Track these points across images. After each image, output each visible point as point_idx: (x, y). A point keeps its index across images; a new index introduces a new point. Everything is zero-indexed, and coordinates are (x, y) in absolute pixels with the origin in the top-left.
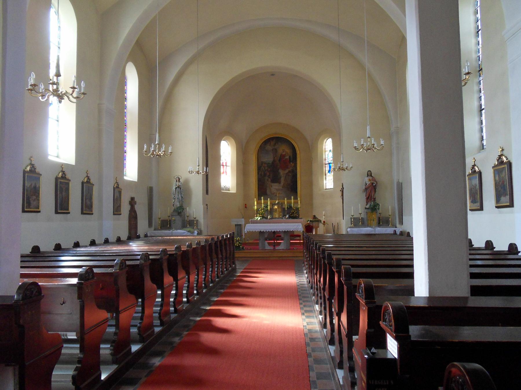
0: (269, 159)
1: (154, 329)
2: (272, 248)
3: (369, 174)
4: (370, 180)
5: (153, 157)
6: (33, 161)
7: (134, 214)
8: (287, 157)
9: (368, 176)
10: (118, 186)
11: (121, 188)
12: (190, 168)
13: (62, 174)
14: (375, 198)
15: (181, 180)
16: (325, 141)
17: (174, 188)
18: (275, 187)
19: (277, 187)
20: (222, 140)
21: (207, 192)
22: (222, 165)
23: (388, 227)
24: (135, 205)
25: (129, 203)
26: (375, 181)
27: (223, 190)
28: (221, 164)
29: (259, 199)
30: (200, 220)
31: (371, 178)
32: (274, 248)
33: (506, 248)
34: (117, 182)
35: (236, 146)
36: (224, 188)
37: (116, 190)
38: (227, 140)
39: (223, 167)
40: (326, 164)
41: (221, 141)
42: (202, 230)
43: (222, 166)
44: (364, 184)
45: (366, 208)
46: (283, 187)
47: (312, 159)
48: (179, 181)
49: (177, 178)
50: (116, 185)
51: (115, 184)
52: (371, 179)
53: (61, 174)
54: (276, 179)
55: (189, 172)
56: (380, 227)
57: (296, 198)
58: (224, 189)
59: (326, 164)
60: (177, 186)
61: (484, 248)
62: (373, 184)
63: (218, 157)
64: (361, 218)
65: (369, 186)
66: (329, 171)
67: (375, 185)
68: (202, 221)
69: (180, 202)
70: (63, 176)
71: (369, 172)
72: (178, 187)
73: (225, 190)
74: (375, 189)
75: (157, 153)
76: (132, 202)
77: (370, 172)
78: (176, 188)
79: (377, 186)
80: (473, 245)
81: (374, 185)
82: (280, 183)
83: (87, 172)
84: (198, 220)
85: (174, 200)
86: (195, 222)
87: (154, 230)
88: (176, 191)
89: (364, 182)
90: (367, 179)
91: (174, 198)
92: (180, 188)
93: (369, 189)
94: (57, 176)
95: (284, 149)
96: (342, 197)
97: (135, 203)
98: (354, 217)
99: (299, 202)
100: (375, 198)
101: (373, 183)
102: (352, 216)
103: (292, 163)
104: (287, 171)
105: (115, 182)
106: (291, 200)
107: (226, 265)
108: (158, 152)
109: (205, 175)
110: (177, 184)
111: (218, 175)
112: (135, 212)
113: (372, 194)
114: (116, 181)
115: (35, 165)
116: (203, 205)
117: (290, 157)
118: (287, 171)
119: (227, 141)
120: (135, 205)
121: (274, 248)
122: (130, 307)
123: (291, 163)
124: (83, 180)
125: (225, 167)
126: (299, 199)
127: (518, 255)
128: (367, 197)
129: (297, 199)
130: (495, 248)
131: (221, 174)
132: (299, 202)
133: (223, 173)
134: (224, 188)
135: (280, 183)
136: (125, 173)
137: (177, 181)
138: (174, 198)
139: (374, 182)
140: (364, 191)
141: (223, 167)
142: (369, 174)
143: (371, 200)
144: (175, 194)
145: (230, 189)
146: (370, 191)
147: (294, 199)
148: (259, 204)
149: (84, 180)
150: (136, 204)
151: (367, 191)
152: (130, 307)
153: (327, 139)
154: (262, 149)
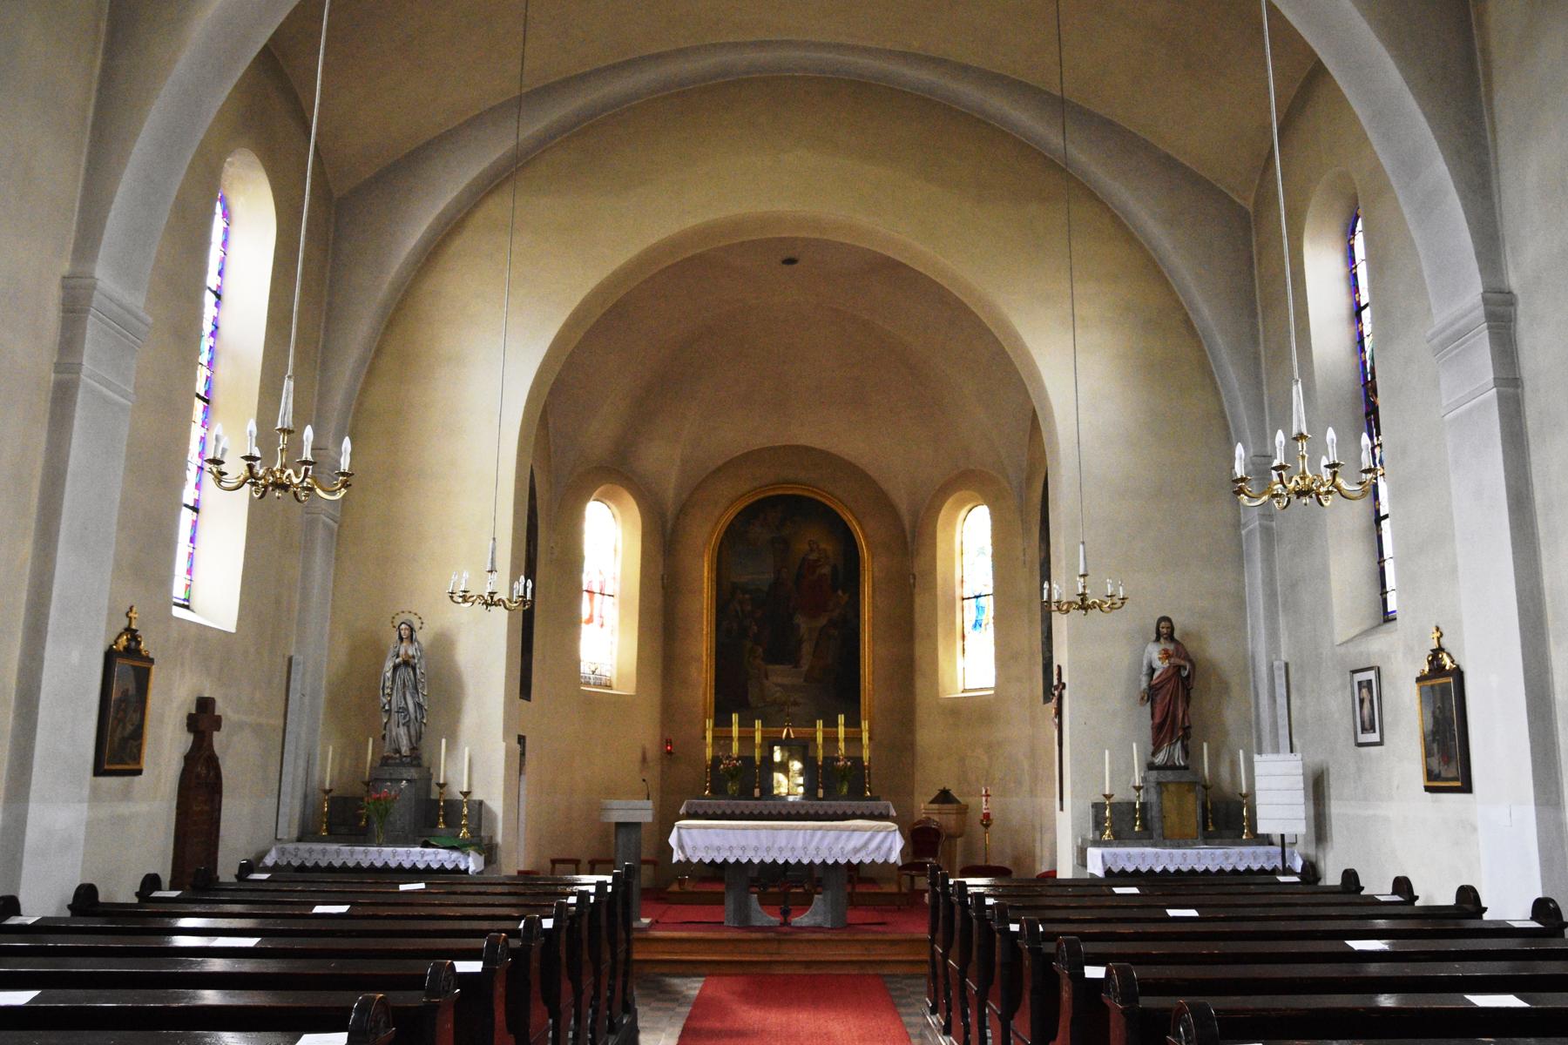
0: (757, 574)
1: (505, 876)
2: (775, 920)
3: (1165, 631)
4: (1166, 655)
5: (261, 497)
6: (134, 622)
7: (209, 772)
8: (826, 570)
9: (1158, 640)
10: (133, 644)
11: (151, 656)
12: (462, 579)
13: (127, 638)
14: (1187, 724)
15: (419, 635)
16: (963, 513)
17: (389, 665)
18: (779, 679)
19: (786, 681)
20: (593, 498)
21: (525, 691)
22: (587, 591)
23: (1238, 840)
24: (215, 733)
25: (185, 721)
26: (1187, 657)
27: (588, 684)
28: (585, 588)
29: (722, 721)
30: (489, 803)
31: (1171, 647)
32: (785, 920)
33: (1448, 899)
34: (134, 627)
35: (643, 523)
36: (592, 676)
37: (121, 665)
38: (610, 500)
39: (591, 600)
40: (963, 599)
41: (588, 500)
42: (497, 845)
43: (585, 595)
44: (1145, 669)
45: (1151, 767)
46: (805, 680)
47: (915, 578)
48: (411, 639)
49: (403, 626)
50: (123, 641)
51: (120, 636)
52: (1171, 653)
53: (125, 637)
54: (782, 651)
55: (451, 597)
56: (1209, 841)
57: (853, 722)
58: (592, 681)
59: (963, 599)
60: (398, 661)
61: (1340, 889)
62: (1179, 670)
63: (571, 562)
64: (1140, 803)
65: (1164, 677)
66: (977, 624)
67: (1188, 676)
68: (496, 802)
69: (408, 727)
70: (129, 644)
71: (1163, 624)
72: (406, 663)
73: (595, 685)
74: (1188, 690)
75: (278, 474)
76: (203, 719)
77: (1168, 624)
78: (396, 668)
79: (1194, 678)
80: (1363, 888)
81: (1185, 673)
82: (797, 664)
83: (130, 615)
84: (481, 803)
85: (387, 716)
86: (465, 811)
87: (299, 840)
88: (393, 681)
89: (1145, 662)
90: (1154, 652)
91: (387, 708)
92: (414, 669)
93: (1164, 691)
94: (111, 646)
95: (812, 542)
96: (1057, 720)
97: (217, 723)
98: (1112, 800)
99: (865, 736)
100: (1189, 727)
101: (1179, 668)
102: (1105, 795)
103: (844, 592)
104: (823, 621)
105: (120, 629)
106: (834, 729)
107: (593, 1031)
108: (282, 472)
109: (521, 613)
110: (402, 652)
111: (570, 622)
112: (213, 763)
113: (1175, 709)
114: (125, 623)
115: (138, 633)
116: (504, 741)
117: (834, 568)
118: (823, 621)
119: (608, 503)
120: (215, 733)
121: (785, 920)
122: (819, 491)
123: (840, 593)
124: (113, 643)
125: (597, 597)
126: (865, 725)
127: (1481, 918)
128: (1157, 720)
129: (858, 725)
130: (1485, 909)
131: (584, 627)
132: (865, 736)
133: (590, 620)
134: (592, 676)
135: (797, 664)
136: (178, 592)
137: (401, 639)
138: (387, 708)
139: (1182, 663)
140: (1146, 698)
141: (591, 600)
142: (1165, 631)
143: (1173, 733)
144: (392, 689)
145: (614, 685)
146: (1168, 697)
147: (846, 725)
148: (722, 739)
149: (116, 643)
150: (218, 728)
151: (1158, 699)
152: (819, 491)
153: (971, 510)
154: (733, 541)
